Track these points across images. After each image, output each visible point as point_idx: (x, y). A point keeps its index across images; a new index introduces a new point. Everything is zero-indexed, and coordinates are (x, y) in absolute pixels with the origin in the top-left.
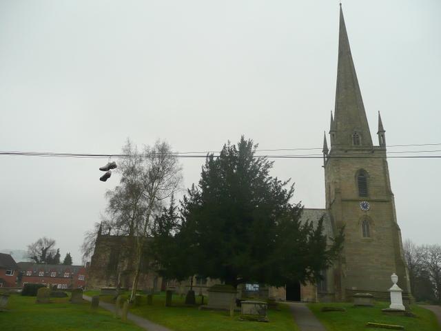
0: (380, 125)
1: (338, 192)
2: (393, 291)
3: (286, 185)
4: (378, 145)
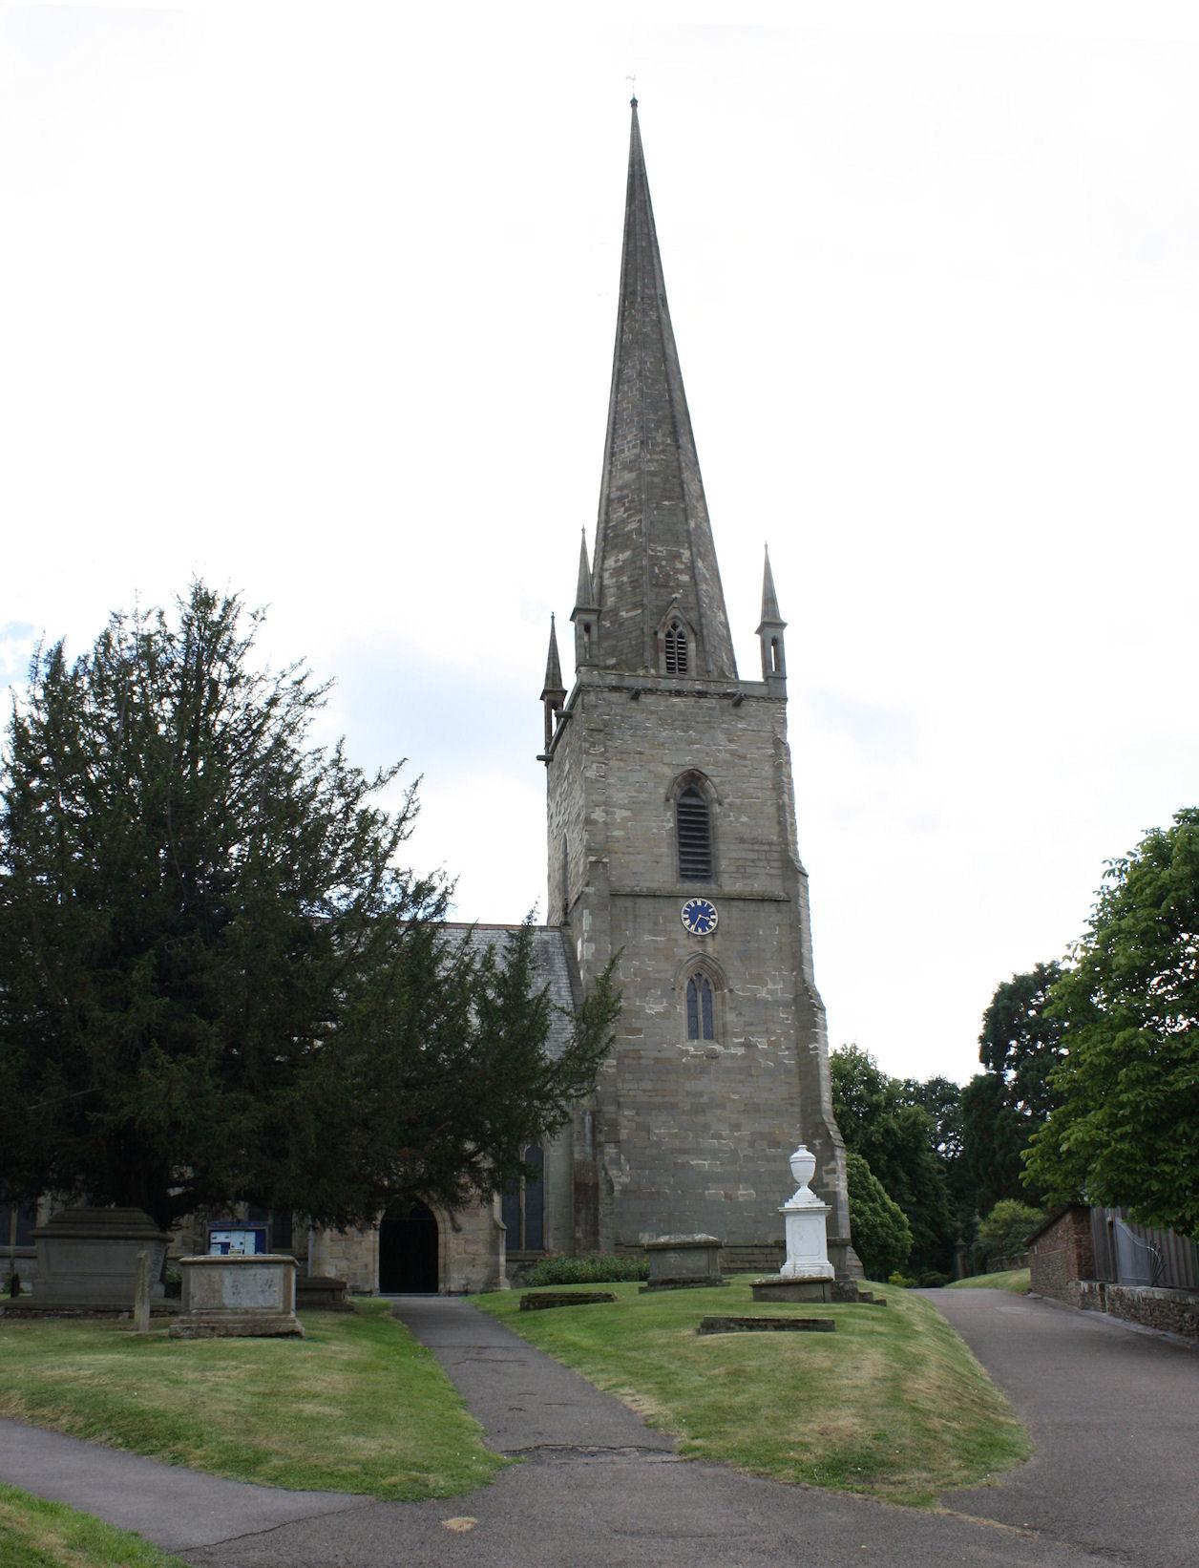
0: (770, 601)
1: (599, 858)
2: (798, 1212)
3: (383, 790)
4: (758, 677)
